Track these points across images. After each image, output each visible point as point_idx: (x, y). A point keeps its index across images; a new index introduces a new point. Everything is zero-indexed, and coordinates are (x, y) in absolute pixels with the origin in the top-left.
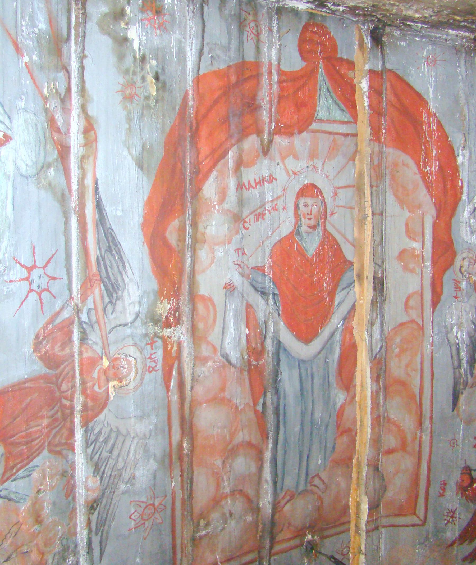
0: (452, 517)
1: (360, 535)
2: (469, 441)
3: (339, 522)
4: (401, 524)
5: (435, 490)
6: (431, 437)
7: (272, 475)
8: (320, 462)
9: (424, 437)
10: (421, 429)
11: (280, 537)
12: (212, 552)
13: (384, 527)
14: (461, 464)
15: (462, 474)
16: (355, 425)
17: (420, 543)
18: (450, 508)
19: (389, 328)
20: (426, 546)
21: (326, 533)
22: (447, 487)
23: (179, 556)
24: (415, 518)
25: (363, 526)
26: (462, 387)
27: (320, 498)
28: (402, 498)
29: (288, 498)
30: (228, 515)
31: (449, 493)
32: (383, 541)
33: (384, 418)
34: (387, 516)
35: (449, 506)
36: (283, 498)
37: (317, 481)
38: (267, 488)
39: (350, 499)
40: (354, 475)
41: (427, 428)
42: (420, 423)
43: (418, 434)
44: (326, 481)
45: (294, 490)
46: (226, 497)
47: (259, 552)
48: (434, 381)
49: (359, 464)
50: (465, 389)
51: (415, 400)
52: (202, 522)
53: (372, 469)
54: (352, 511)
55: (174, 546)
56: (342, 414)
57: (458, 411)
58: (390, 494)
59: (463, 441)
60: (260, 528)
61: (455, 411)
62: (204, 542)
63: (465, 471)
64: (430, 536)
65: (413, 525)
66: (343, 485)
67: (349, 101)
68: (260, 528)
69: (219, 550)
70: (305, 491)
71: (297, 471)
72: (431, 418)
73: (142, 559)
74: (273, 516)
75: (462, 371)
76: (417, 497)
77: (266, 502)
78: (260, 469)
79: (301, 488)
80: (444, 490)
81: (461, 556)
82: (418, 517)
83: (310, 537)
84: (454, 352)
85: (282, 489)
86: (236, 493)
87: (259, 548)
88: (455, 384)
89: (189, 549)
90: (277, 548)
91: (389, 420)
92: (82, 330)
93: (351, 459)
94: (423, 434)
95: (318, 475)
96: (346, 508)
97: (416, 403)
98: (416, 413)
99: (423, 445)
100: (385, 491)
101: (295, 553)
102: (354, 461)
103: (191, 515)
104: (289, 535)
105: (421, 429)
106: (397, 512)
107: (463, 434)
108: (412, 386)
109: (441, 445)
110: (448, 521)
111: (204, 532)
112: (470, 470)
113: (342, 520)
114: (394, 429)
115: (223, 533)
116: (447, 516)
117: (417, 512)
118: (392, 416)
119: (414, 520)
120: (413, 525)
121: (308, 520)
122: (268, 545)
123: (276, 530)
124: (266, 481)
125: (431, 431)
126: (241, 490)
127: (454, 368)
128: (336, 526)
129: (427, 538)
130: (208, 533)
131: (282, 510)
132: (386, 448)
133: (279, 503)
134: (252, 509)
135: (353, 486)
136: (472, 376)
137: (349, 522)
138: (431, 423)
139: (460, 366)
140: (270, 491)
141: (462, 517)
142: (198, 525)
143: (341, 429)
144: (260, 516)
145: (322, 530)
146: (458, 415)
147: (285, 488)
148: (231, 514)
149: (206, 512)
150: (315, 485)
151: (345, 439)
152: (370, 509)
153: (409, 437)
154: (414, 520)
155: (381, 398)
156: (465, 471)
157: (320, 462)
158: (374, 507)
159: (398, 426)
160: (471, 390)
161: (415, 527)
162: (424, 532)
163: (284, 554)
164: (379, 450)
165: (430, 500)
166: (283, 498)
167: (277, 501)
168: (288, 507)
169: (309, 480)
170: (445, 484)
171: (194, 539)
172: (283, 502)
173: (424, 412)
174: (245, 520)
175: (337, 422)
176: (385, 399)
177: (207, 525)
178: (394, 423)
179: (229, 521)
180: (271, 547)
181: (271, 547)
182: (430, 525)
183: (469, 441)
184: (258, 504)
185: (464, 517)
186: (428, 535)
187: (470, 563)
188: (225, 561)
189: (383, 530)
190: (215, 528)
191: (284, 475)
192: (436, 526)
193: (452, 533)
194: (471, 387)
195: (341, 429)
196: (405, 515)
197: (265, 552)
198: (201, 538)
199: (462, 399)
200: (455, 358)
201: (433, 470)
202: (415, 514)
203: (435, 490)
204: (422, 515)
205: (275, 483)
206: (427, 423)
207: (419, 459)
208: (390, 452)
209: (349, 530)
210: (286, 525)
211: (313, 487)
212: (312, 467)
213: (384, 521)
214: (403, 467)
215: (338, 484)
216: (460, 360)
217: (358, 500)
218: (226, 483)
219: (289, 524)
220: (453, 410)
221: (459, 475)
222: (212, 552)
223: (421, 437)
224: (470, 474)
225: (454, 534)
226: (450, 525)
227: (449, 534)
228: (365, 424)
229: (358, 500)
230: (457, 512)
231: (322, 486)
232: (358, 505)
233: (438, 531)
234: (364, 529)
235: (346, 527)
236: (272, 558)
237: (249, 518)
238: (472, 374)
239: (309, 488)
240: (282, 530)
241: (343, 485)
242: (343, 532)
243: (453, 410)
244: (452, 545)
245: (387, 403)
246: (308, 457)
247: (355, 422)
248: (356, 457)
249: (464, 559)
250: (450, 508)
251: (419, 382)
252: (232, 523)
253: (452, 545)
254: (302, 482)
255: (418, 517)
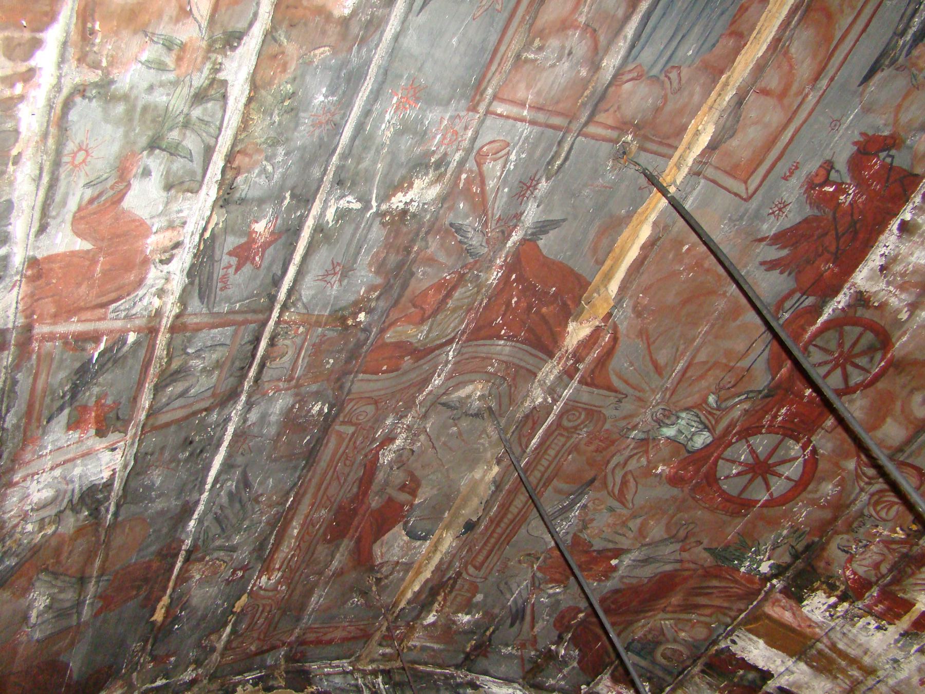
0: (780, 210)
1: (679, 168)
2: (853, 132)
3: (343, 459)
4: (724, 185)
5: (782, 168)
6: (818, 102)
7: (634, 34)
8: (691, 52)
9: (810, 97)
10: (813, 86)
11: (601, 117)
12: (528, 87)
13: (706, 178)
14: (827, 155)
15: (821, 166)
16: (750, 34)
17: (730, 219)
18: (785, 198)
19: (142, 450)
20: (735, 225)
21: (649, 145)
22: (797, 172)
23: (493, 68)
24: (743, 187)
25: (690, 161)
26: (887, 63)
27: (665, 98)
28: (745, 155)
29: (635, 74)
30: (567, 52)
31: (793, 181)
32: (695, 193)
33: (783, 46)
34: (717, 168)
35: (785, 196)
36: (630, 71)
37: (673, 75)
38: (622, 46)
39: (693, 122)
40: (713, 95)
41: (820, 88)
42: (817, 78)
43: (807, 90)
44: (683, 81)
45: (646, 68)
46: (576, 28)
47: (570, 122)
48: (864, 35)
49: (726, 84)
50: (889, 66)
51: (829, 47)
52: (537, 42)
53: (736, 99)
54: (687, 137)
55: (496, 51)
56: (746, 9)
57: (864, 91)
58: (734, 142)
59: (848, 128)
60: (587, 93)
61: (861, 87)
62: (528, 67)
63: (825, 166)
64: (746, 218)
65: (736, 195)
66: (696, 98)
67: (625, 43)
68: (587, 93)
69: (536, 90)
70: (655, 79)
71: (662, 47)
72: (832, 79)
73: (459, 42)
74: (610, 84)
75: (901, 43)
76: (758, 165)
77: (611, 63)
78: (627, 18)
79: (655, 72)
80: (792, 173)
81: (760, 259)
82: (747, 189)
83: (630, 137)
84: (909, 12)
85: (635, 59)
86: (589, 30)
87: (572, 117)
88: (883, 54)
89: (508, 66)
90: (591, 129)
91: (786, 53)
92: (347, 152)
93: (722, 72)
94: (812, 94)
95: (679, 68)
96: (684, 129)
97: (828, 49)
98: (821, 62)
99: (803, 107)
100: (731, 137)
101: (606, 147)
102: (724, 78)
103: (531, 25)
104: (610, 122)
105: (813, 86)
106: (728, 169)
107: (852, 120)
108: (837, 26)
109: (821, 119)
110: (773, 213)
111: (532, 56)
112: (832, 168)
113: (670, 141)
114: (786, 68)
115: (550, 70)
116: (776, 205)
117: (749, 181)
118: (793, 50)
119: (739, 188)
120: (736, 195)
121: (639, 116)
122: (583, 119)
123: (603, 106)
124: (625, 37)
125: (823, 94)
126: (595, 30)
127: (895, 33)
128: (661, 143)
129: (741, 218)
130: (536, 60)
131: (620, 85)
132: (763, 85)
133: (623, 74)
134: (593, 63)
135: (705, 108)
136: (907, 55)
137: (676, 148)
138: (828, 86)
139: (903, 33)
140: (622, 52)
141: (791, 215)
142: (532, 42)
143: (733, 28)
144: (595, 78)
145: (646, 138)
146: (862, 94)
147: (638, 61)
148: (570, 53)
149: (547, 31)
150: (669, 78)
151: (731, 42)
152: (708, 147)
153: (795, 88)
154: (739, 188)
155: (796, 18)
156: (825, 166)
157: (691, 52)
158: (712, 147)
159: (791, 67)
160: (894, 72)
161: (737, 198)
162: (742, 210)
163: (593, 142)
164: (755, 82)
165: (771, 176)
166: (630, 71)
167: (621, 72)
168: (628, 86)
169: (666, 69)
170: (797, 168)
171: (518, 56)
172: (625, 78)
173: (829, 66)
174: (579, 72)
175: (735, 16)
176: (800, 21)
177: (541, 49)
178: (790, 59)
179: (563, 60)
180: (586, 124)
181: (586, 124)
182: (754, 204)
183: (853, 132)
184: (602, 59)
185: (792, 218)
186: (744, 214)
187: (766, 270)
188: (534, 107)
189: (702, 181)
190: (546, 59)
191: (647, 42)
192: (758, 210)
193: (769, 227)
194: (897, 69)
195: (733, 28)
196: (735, 177)
197: (575, 126)
198: (527, 61)
199: (879, 76)
200: (905, 20)
201: (795, 141)
202: (745, 182)
203: (782, 168)
204: (752, 188)
205: (632, 46)
206: (824, 83)
207: (790, 120)
208: (765, 92)
209: (670, 157)
210: (615, 107)
211: (666, 79)
212: (680, 53)
213: (710, 172)
214: (767, 119)
215: (691, 95)
216: (908, 26)
217: (700, 128)
218: (586, 10)
219: (619, 108)
220: (859, 85)
221: (818, 166)
222: (528, 87)
223: (807, 95)
224: (829, 172)
225: (771, 230)
226: (772, 217)
227: (765, 226)
228: (763, 37)
229: (700, 128)
230: (788, 208)
231: (675, 84)
232: (697, 133)
233: (757, 216)
234: (690, 164)
235: (670, 151)
236: (580, 137)
237: (584, 73)
238: (909, 53)
239: (662, 77)
240: (607, 110)
241: (696, 98)
242: (664, 156)
243: (859, 85)
244: (762, 240)
245: (797, 31)
246: (683, 37)
247: (752, 29)
248: (729, 73)
249: (762, 263)
250: (785, 198)
251: (846, 26)
252: (566, 65)
253: (762, 240)
254: (659, 66)
255: (747, 189)
